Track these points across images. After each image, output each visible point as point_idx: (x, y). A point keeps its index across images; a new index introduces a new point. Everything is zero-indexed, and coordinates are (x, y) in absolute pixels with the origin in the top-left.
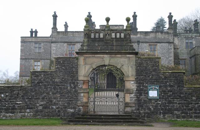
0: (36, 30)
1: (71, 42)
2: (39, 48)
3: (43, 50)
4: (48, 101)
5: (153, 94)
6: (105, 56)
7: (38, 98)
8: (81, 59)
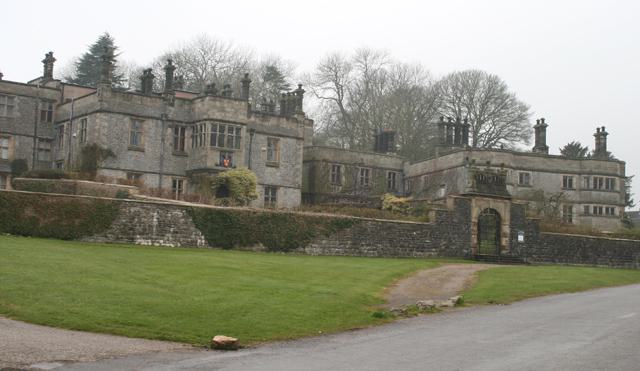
3: (19, 114)
5: (521, 238)
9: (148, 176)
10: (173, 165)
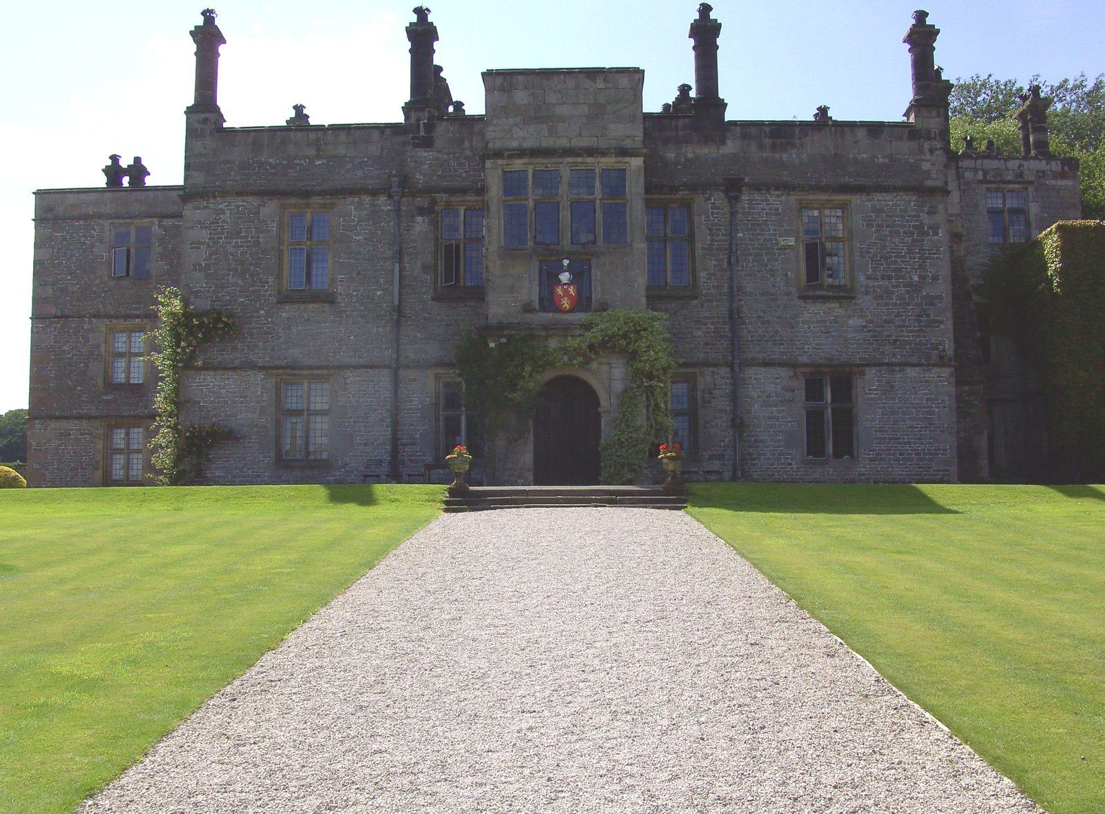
0: (137, 160)
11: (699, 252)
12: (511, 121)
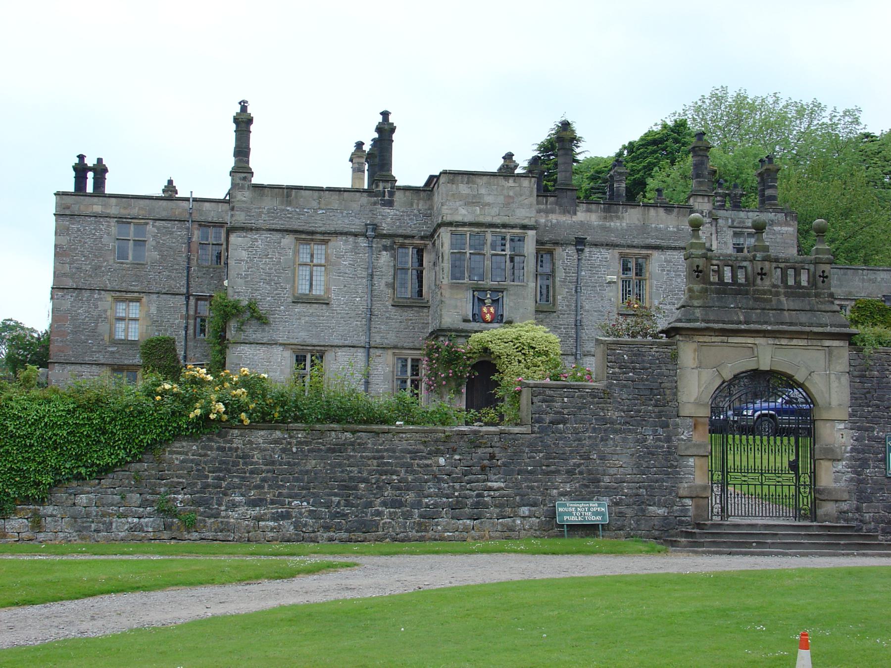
0: (100, 160)
1: (313, 233)
2: (135, 245)
3: (156, 255)
4: (585, 482)
6: (760, 341)
7: (554, 472)
8: (688, 352)
9: (340, 353)
10: (393, 327)
11: (558, 284)
12: (458, 203)
